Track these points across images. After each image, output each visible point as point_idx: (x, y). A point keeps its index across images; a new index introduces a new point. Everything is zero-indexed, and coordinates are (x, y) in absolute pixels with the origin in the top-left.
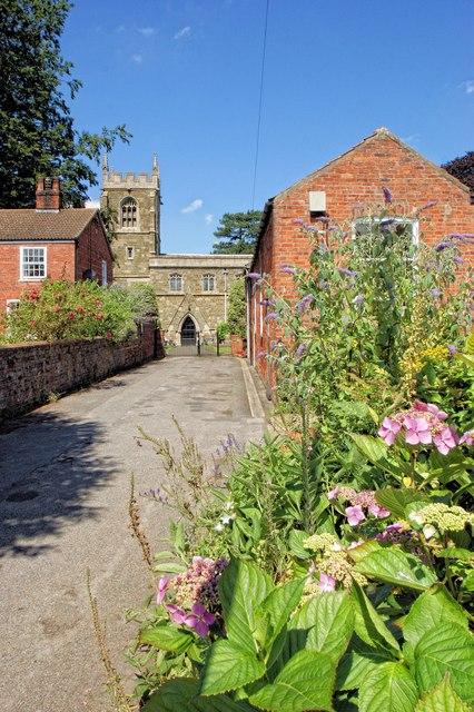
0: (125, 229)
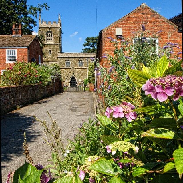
0: (48, 43)
